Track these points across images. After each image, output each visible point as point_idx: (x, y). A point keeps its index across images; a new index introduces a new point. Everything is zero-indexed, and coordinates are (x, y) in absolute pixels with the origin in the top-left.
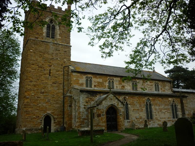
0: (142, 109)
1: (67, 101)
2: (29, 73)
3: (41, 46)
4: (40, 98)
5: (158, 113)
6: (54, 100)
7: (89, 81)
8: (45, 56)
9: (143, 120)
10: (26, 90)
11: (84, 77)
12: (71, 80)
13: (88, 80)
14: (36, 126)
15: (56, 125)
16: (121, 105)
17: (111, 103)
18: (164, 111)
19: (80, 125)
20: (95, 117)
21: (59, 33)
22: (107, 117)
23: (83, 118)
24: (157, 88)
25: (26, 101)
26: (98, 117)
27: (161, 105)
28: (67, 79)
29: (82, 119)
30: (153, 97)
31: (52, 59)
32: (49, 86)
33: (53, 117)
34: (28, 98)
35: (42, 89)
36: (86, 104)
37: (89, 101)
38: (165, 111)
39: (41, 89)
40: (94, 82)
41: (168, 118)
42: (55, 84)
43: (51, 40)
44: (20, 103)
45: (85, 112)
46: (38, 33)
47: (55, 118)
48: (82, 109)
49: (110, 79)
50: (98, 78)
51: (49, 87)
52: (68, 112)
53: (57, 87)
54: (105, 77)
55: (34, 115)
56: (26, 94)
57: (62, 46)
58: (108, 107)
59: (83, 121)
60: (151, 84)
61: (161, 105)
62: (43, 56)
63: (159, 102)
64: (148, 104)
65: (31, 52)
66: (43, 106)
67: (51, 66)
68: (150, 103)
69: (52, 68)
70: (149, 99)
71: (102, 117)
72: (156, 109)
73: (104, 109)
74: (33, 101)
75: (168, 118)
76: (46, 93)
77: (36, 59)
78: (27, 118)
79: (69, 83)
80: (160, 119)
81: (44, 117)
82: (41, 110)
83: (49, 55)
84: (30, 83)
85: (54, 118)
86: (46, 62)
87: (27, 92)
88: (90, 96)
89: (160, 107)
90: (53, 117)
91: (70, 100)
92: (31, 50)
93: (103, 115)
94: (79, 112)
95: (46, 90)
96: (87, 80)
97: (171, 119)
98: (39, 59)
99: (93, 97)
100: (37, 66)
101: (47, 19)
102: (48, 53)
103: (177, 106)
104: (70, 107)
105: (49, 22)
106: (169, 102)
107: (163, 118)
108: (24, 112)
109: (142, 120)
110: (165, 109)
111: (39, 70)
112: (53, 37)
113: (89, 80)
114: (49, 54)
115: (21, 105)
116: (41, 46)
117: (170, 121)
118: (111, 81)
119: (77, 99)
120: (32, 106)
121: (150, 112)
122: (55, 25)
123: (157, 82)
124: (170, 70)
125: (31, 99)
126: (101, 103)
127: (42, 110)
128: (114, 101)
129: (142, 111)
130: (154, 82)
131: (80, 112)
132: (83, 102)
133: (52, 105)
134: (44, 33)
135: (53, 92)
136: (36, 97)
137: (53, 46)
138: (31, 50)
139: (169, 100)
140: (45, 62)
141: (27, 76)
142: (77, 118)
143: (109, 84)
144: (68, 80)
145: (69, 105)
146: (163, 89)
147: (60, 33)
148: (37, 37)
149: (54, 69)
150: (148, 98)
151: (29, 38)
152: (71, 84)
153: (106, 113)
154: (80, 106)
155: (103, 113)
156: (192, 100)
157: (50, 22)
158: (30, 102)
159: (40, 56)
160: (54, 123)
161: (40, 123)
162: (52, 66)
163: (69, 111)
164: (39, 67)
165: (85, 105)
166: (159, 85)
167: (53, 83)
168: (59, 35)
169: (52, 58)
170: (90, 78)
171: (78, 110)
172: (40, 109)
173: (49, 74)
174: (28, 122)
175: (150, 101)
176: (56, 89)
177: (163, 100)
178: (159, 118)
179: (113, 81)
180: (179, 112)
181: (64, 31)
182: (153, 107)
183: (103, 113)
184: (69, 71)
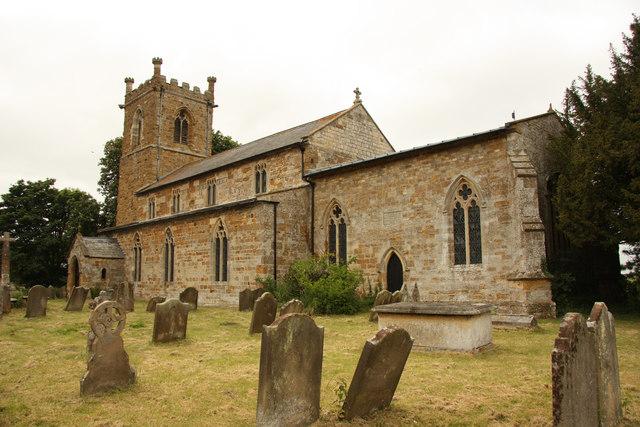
0: (158, 259)
18: (194, 259)
41: (203, 279)
75: (203, 279)
89: (190, 249)
97: (209, 283)
110: (198, 254)
117: (205, 287)
124: (59, 186)
156: (393, 193)
182: (175, 248)
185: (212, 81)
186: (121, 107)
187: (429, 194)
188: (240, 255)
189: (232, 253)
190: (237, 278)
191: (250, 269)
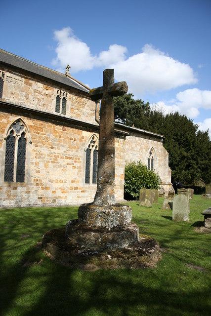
18: (61, 162)
38: (68, 164)
41: (73, 182)
60: (47, 92)
89: (53, 151)
110: (67, 158)
117: (76, 188)
139: (83, 137)
182: (29, 148)
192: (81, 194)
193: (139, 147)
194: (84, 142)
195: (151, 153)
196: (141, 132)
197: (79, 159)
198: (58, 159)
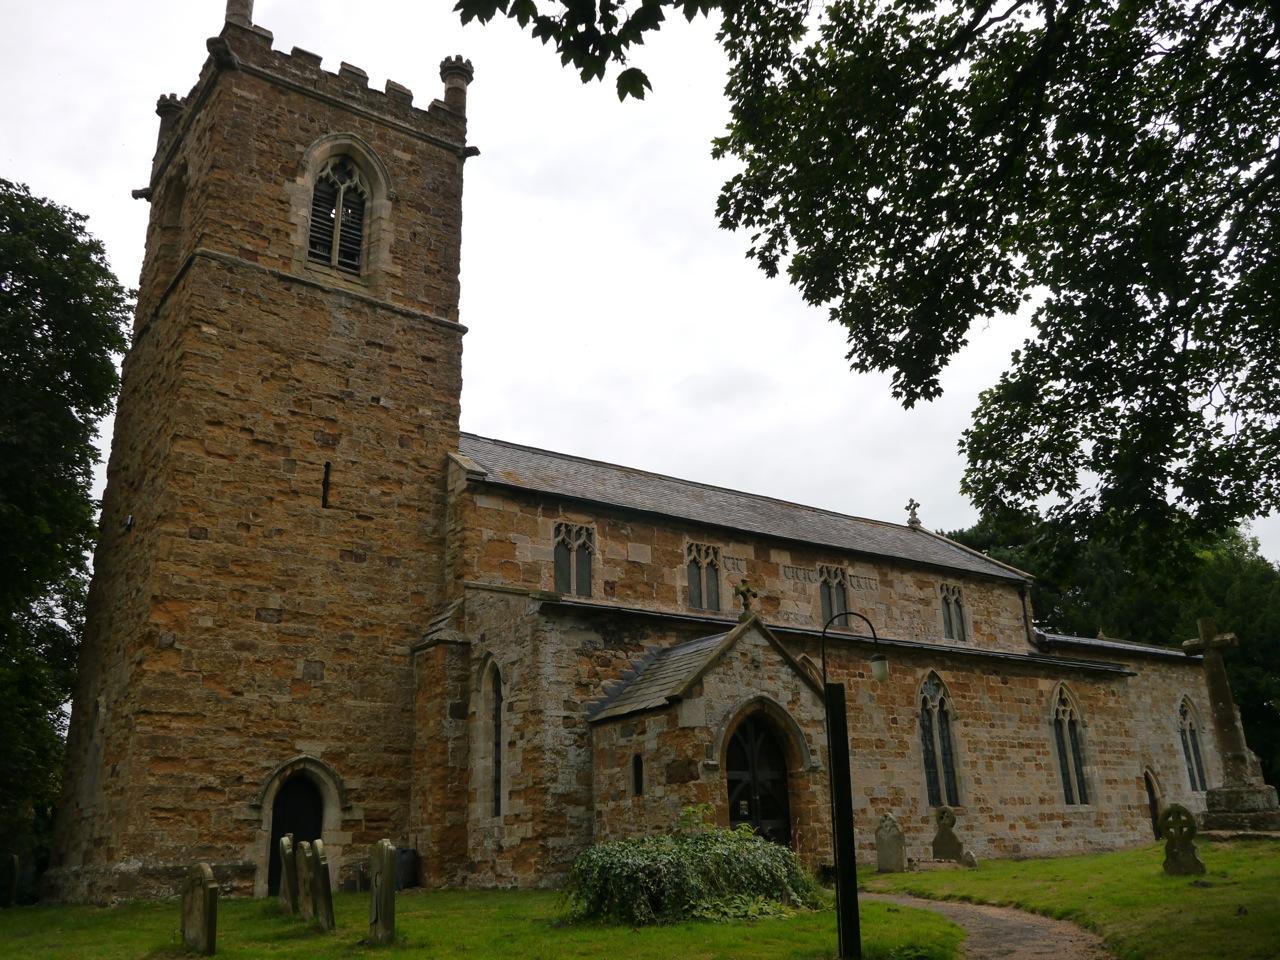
0: (903, 744)
1: (450, 670)
2: (190, 479)
3: (272, 307)
4: (250, 647)
5: (987, 767)
6: (351, 669)
7: (573, 555)
8: (296, 372)
9: (907, 808)
10: (158, 593)
11: (547, 524)
12: (467, 542)
13: (570, 550)
14: (219, 845)
15: (354, 840)
16: (815, 704)
17: (756, 692)
18: (1016, 756)
19: (536, 838)
20: (645, 784)
21: (389, 238)
22: (732, 785)
23: (560, 791)
24: (955, 623)
25: (154, 667)
26: (670, 780)
27: (1001, 718)
28: (433, 533)
29: (554, 794)
30: (959, 669)
31: (342, 400)
32: (318, 573)
33: (340, 784)
34: (171, 646)
35: (267, 589)
36: (577, 699)
37: (596, 674)
38: (1026, 759)
39: (261, 589)
40: (607, 562)
41: (1042, 801)
42: (360, 558)
43: (335, 280)
44: (105, 682)
45: (572, 752)
46: (260, 226)
47: (354, 795)
48: (551, 731)
49: (699, 551)
50: (628, 538)
51: (319, 582)
52: (444, 753)
53: (370, 580)
54: (669, 535)
55: (209, 766)
56: (158, 618)
57: (406, 322)
58: (739, 713)
59: (560, 815)
60: (922, 595)
61: (1001, 718)
62: (283, 372)
63: (987, 700)
64: (929, 713)
65: (208, 340)
66: (274, 706)
67: (336, 439)
68: (942, 702)
69: (341, 455)
70: (936, 681)
71: (703, 780)
72: (974, 745)
73: (714, 730)
74: (207, 667)
76: (296, 616)
77: (237, 387)
78: (158, 790)
79: (448, 558)
80: (1001, 809)
81: (276, 784)
82: (255, 735)
83: (326, 371)
84: (187, 546)
85: (345, 794)
86: (306, 411)
87: (167, 603)
88: (600, 644)
89: (996, 732)
90: (340, 784)
91: (455, 674)
92: (205, 329)
93: (707, 767)
94: (529, 747)
95: (299, 599)
96: (563, 547)
98: (259, 392)
99: (621, 654)
100: (245, 436)
101: (321, 149)
102: (317, 359)
103: (1079, 728)
104: (461, 718)
105: (328, 170)
106: (1039, 702)
107: (1013, 801)
108: (140, 742)
109: (904, 812)
110: (1021, 745)
111: (256, 462)
112: (352, 257)
113: (575, 545)
114: (325, 365)
115: (114, 697)
116: (272, 307)
117: (1051, 817)
118: (704, 563)
119: (513, 663)
120: (198, 708)
121: (945, 761)
122: (367, 190)
123: (951, 582)
125: (189, 653)
126: (697, 687)
127: (268, 736)
128: (770, 678)
129: (902, 755)
130: (938, 581)
131: (538, 749)
132: (558, 683)
133: (332, 699)
134: (296, 231)
135: (345, 618)
136: (228, 644)
137: (353, 316)
138: (204, 329)
139: (1041, 693)
140: (293, 413)
141: (172, 496)
142: (511, 793)
143: (690, 580)
144: (442, 542)
145: (448, 703)
146: (984, 627)
147: (398, 241)
148: (248, 247)
149: (354, 463)
150: (933, 675)
151: (198, 250)
152: (466, 563)
153: (729, 751)
154: (537, 712)
155: (711, 757)
157: (332, 169)
158: (185, 675)
159: (268, 372)
160: (346, 825)
161: (249, 822)
162: (344, 442)
163: (450, 745)
164: (257, 442)
165: (569, 705)
166: (964, 602)
167: (347, 554)
168: (391, 252)
169: (343, 392)
170: (579, 533)
171: (522, 737)
172: (254, 729)
173: (321, 493)
174: (162, 815)
175: (941, 692)
176: (363, 594)
177: (1011, 689)
178: (993, 802)
179: (711, 565)
180: (1095, 768)
181: (420, 229)
182: (957, 729)
183: (711, 757)
184: (450, 479)
185: (912, 506)
186: (474, 151)
187: (1163, 706)
188: (1107, 757)
189: (1091, 751)
190: (1109, 798)
191: (1126, 782)
192: (1063, 832)
193: (1147, 699)
194: (1044, 704)
195: (1184, 713)
196: (1114, 649)
197: (1043, 746)
198: (1007, 749)
